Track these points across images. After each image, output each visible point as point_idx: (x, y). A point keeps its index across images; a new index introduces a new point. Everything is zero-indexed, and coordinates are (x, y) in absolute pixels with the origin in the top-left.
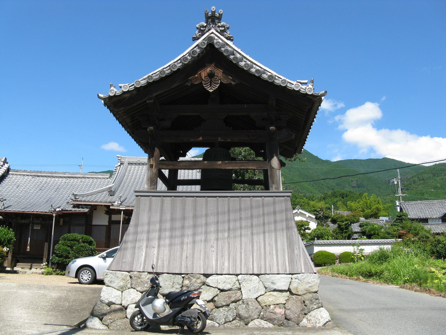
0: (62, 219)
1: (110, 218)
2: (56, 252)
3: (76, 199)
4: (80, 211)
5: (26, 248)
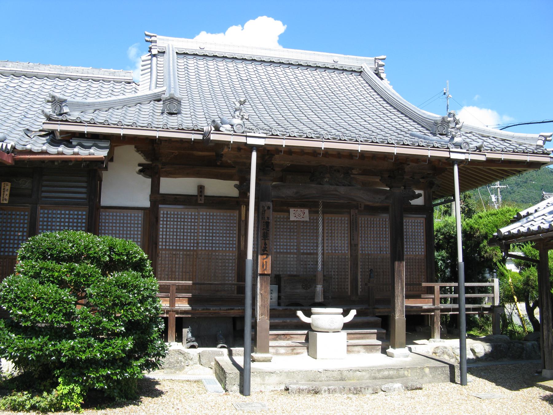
0: (9, 184)
1: (155, 187)
2: (6, 312)
3: (61, 115)
4: (78, 154)
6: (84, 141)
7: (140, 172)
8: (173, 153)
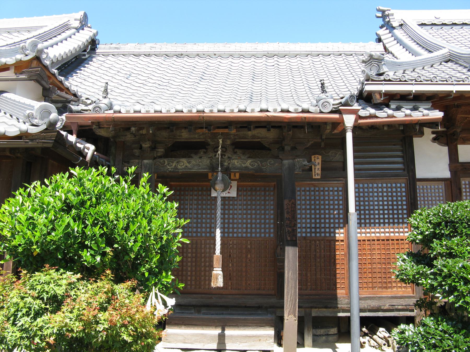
0: (320, 157)
1: (453, 155)
5: (209, 277)
6: (420, 104)
7: (434, 140)
8: (466, 118)
